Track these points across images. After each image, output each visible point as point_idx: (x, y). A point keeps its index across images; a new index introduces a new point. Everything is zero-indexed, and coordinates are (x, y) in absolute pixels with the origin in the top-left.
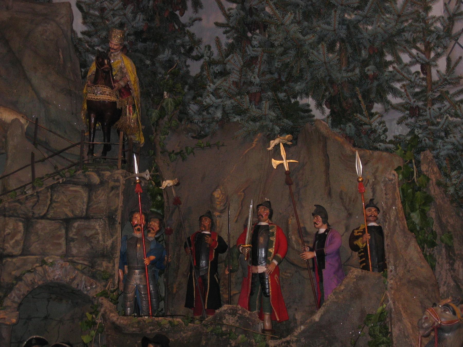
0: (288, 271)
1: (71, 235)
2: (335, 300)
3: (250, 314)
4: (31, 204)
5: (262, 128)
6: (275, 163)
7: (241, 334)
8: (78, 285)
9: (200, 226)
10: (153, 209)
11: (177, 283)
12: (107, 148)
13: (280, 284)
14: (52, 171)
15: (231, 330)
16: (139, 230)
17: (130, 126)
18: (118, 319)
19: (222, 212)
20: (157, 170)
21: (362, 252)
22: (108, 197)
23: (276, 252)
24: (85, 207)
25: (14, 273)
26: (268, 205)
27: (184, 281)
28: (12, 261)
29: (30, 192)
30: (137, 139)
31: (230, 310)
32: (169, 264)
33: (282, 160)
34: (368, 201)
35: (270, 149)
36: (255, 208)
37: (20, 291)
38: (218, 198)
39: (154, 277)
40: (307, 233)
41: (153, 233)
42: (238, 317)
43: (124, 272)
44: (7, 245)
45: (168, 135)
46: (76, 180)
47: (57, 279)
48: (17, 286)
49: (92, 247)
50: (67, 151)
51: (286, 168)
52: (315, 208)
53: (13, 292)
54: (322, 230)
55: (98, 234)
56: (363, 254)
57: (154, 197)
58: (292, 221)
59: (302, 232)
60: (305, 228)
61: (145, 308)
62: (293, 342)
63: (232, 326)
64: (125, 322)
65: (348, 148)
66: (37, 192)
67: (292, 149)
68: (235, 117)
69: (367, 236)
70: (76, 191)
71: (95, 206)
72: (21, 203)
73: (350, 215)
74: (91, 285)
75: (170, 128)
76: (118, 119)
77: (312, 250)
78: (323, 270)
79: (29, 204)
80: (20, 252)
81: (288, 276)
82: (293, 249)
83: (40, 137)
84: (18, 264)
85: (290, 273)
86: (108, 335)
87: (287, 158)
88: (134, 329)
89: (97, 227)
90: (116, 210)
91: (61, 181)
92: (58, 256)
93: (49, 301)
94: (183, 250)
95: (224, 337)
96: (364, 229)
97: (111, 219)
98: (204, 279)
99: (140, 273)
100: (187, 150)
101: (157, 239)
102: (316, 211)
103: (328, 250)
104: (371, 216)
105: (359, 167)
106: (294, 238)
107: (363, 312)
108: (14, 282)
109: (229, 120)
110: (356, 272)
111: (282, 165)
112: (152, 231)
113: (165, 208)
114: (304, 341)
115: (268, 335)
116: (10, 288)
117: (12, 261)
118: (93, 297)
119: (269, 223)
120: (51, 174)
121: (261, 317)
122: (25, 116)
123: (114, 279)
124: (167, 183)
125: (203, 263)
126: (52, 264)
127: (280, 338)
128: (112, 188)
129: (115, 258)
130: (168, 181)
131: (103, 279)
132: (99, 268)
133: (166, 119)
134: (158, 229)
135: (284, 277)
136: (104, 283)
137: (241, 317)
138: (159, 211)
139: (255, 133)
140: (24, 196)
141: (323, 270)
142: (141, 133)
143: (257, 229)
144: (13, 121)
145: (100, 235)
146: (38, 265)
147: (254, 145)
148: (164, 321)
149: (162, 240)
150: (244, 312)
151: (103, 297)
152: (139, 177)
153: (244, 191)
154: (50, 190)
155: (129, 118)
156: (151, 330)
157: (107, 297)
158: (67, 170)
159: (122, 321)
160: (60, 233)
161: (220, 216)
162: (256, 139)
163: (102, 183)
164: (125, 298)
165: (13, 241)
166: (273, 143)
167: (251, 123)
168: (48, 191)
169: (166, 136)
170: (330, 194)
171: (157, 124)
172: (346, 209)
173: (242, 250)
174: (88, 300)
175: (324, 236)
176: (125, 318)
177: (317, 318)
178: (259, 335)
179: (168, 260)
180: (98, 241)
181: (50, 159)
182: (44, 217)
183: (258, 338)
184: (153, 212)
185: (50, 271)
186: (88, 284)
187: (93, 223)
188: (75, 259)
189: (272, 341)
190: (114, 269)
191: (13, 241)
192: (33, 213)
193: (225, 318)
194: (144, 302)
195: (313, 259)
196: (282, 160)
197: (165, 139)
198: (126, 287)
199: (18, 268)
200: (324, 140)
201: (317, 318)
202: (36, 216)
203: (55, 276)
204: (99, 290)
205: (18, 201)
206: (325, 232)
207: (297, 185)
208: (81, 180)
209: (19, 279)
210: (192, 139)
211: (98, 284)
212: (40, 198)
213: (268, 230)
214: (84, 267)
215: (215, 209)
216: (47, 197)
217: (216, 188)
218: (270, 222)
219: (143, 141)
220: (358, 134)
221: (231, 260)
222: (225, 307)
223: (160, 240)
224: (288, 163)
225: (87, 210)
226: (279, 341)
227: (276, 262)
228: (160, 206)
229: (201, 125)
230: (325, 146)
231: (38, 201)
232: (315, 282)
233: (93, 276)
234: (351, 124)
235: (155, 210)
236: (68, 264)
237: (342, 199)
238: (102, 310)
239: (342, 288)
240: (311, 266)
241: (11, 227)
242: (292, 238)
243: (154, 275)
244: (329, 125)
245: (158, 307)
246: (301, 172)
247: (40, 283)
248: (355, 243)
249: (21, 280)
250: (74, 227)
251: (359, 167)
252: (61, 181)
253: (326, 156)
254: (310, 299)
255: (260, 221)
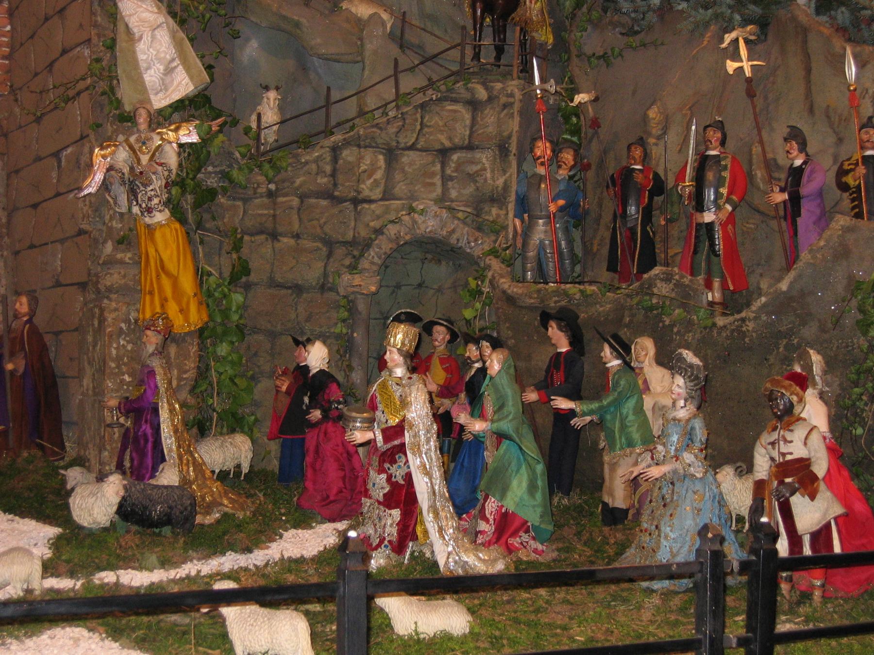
0: (751, 221)
1: (448, 172)
2: (812, 261)
3: (691, 281)
4: (395, 130)
5: (716, 16)
6: (731, 66)
7: (679, 307)
8: (458, 240)
9: (628, 157)
10: (565, 136)
11: (598, 238)
12: (500, 51)
13: (735, 238)
14: (425, 83)
15: (664, 303)
16: (542, 164)
17: (531, 19)
18: (510, 286)
19: (659, 138)
20: (572, 81)
21: (854, 192)
22: (499, 119)
23: (730, 193)
24: (468, 133)
25: (372, 224)
26: (720, 126)
27: (608, 235)
28: (369, 208)
29: (392, 114)
30: (543, 39)
31: (663, 274)
32: (586, 213)
33: (742, 61)
34: (865, 120)
35: (724, 45)
36: (701, 130)
37: (380, 248)
38: (654, 119)
39: (566, 230)
40: (778, 167)
41: (565, 169)
42: (675, 284)
43: (523, 221)
44: (363, 186)
45: (586, 31)
46: (454, 95)
47: (430, 232)
48: (377, 242)
49: (478, 189)
50: (441, 56)
51: (748, 73)
52: (788, 130)
53: (371, 250)
54: (798, 162)
55: (485, 170)
56: (855, 195)
57: (567, 118)
58: (757, 150)
59: (770, 165)
60: (775, 160)
61: (551, 273)
62: (750, 320)
63: (664, 296)
64: (520, 291)
65: (837, 43)
66: (402, 114)
67: (759, 47)
68: (679, 4)
69: (861, 170)
70: (455, 111)
71: (480, 132)
72: (381, 129)
73: (840, 140)
74: (476, 240)
75: (590, 21)
76: (515, 9)
77: (782, 190)
78: (798, 219)
79: (392, 129)
80: (380, 196)
81: (751, 228)
82: (759, 189)
83: (411, 37)
84: (378, 212)
85: (754, 224)
86: (498, 308)
87: (749, 60)
88: (532, 301)
89: (484, 160)
90: (510, 137)
91: (434, 97)
92: (431, 200)
93: (423, 263)
94: (605, 194)
95: (655, 312)
96: (857, 160)
97: (503, 150)
98: (632, 231)
99: (544, 224)
100: (613, 54)
101: (571, 178)
102: (790, 134)
103: (807, 189)
104: (868, 141)
105: (851, 70)
106: (759, 174)
107: (851, 278)
108: (373, 236)
109: (672, 8)
110: (842, 221)
111: (741, 68)
112: (564, 166)
113: (583, 135)
114: (765, 318)
115: (718, 309)
116: (367, 245)
117: (369, 208)
118: (479, 257)
119: (721, 153)
120: (420, 89)
121: (709, 286)
122: (388, 9)
123: (507, 232)
124: (581, 98)
125: (632, 209)
126: (422, 212)
127: (732, 314)
128: (505, 106)
129: (508, 203)
130: (582, 95)
131: (492, 232)
132: (487, 217)
133: (584, 9)
134: (572, 163)
135: (745, 229)
136: (493, 238)
137: (678, 285)
138: (575, 139)
139: (707, 24)
140: (385, 119)
141: (798, 219)
142: (549, 29)
143: (703, 162)
144: (371, 16)
145: (489, 171)
146: (404, 213)
147: (705, 43)
148: (572, 289)
149: (579, 180)
150: (682, 277)
151: (491, 257)
152: (541, 90)
153: (690, 108)
154: (419, 110)
155: (530, 8)
156: (556, 302)
157: (497, 257)
158: (442, 82)
159: (516, 290)
160: (433, 169)
161: (656, 145)
162: (709, 34)
163: (490, 99)
164: (525, 258)
165: (372, 180)
166: (728, 38)
167: (701, 10)
168: (417, 112)
169: (584, 33)
170: (811, 110)
171: (573, 16)
172: (835, 132)
173: (681, 190)
174: (473, 261)
175: (799, 171)
176: (520, 285)
177: (784, 286)
178: (703, 310)
179: (584, 205)
180: (486, 180)
181: (421, 67)
182: (412, 148)
183: (702, 313)
184: (566, 140)
185: (420, 222)
186: (472, 239)
187: (478, 155)
188: (454, 205)
189: (721, 318)
190: (507, 218)
191: (372, 180)
192: (398, 142)
193: (656, 286)
194: (551, 264)
195: (785, 202)
196: (742, 61)
197: (581, 37)
198: (525, 244)
199: (378, 217)
200: (804, 32)
201: (784, 286)
202: (402, 145)
203: (427, 228)
204: (487, 247)
205: (377, 126)
206: (802, 164)
207: (766, 98)
208: (462, 96)
209: (379, 232)
210: (620, 36)
211: (486, 239)
212: (407, 121)
213: (720, 162)
214: (466, 214)
215: (649, 134)
216: (416, 120)
217: (652, 105)
218: (722, 150)
219: (551, 41)
220: (856, 23)
221: (669, 206)
222: (657, 270)
223: (576, 178)
224: (752, 66)
225: (470, 136)
226: (731, 319)
227: (729, 208)
228: (576, 131)
229: (633, 15)
230: (805, 42)
231: (403, 126)
232: (787, 236)
233: (479, 229)
234: (843, 9)
235: (569, 137)
236: (444, 211)
237: (828, 117)
238: (490, 274)
239: (822, 243)
240: (782, 213)
241: (368, 162)
242: (756, 174)
243: (567, 227)
244: (812, 11)
245: (573, 271)
246: (772, 79)
247: (408, 238)
248: (844, 179)
249: (383, 233)
250: (452, 160)
251: (851, 70)
252: (434, 97)
253: (807, 57)
254: (779, 260)
255: (707, 149)
